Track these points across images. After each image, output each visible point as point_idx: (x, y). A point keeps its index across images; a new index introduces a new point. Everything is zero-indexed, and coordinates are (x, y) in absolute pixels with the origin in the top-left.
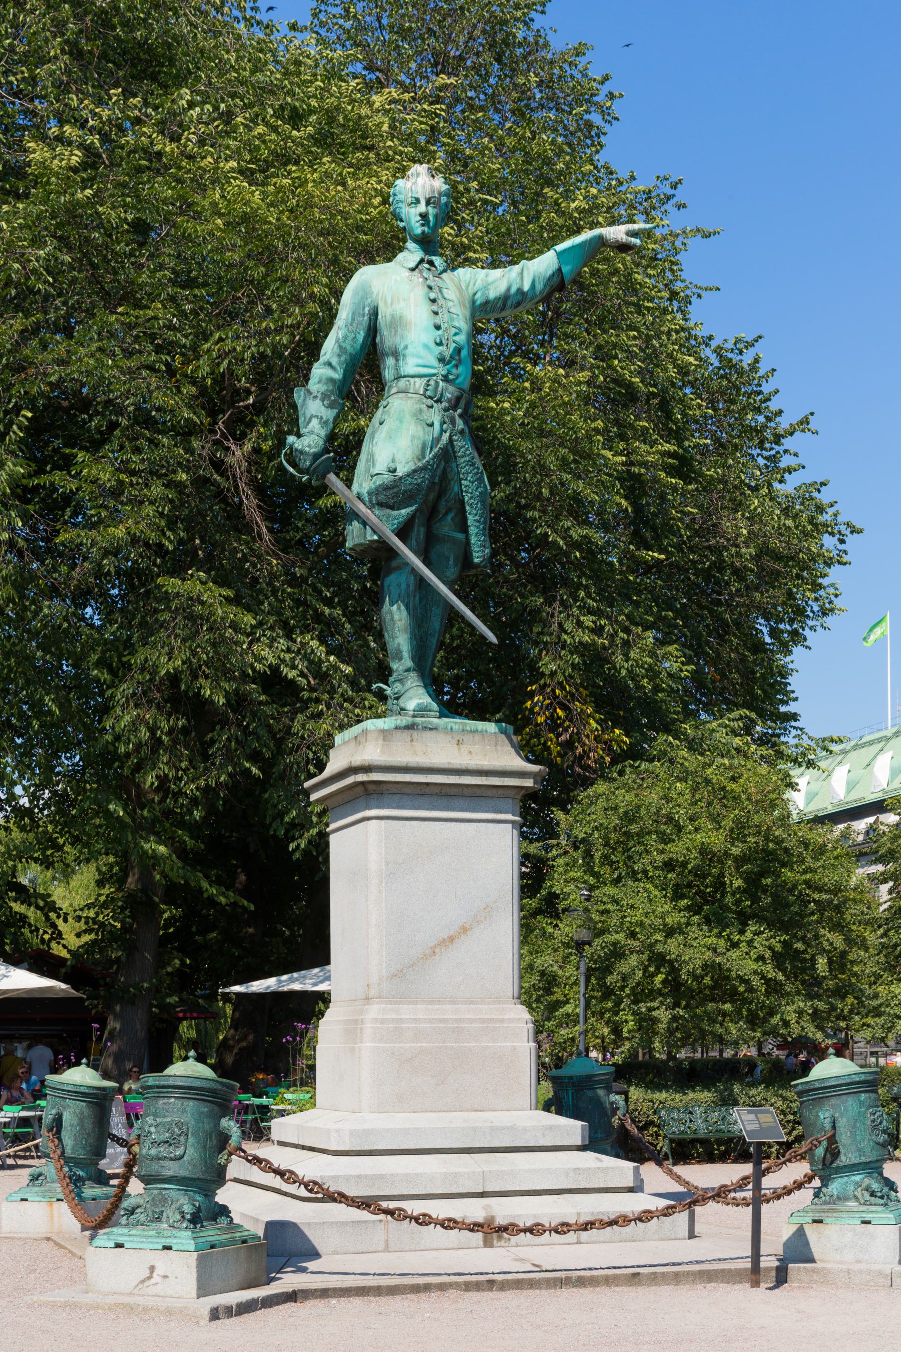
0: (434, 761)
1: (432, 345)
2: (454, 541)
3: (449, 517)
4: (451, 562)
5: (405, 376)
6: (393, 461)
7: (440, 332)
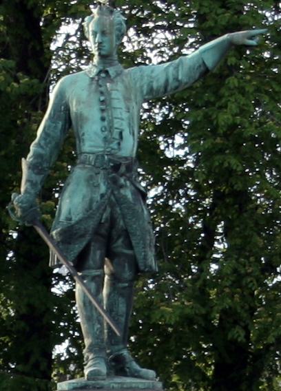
1: (99, 131)
2: (126, 255)
5: (84, 153)
6: (70, 213)
7: (106, 123)
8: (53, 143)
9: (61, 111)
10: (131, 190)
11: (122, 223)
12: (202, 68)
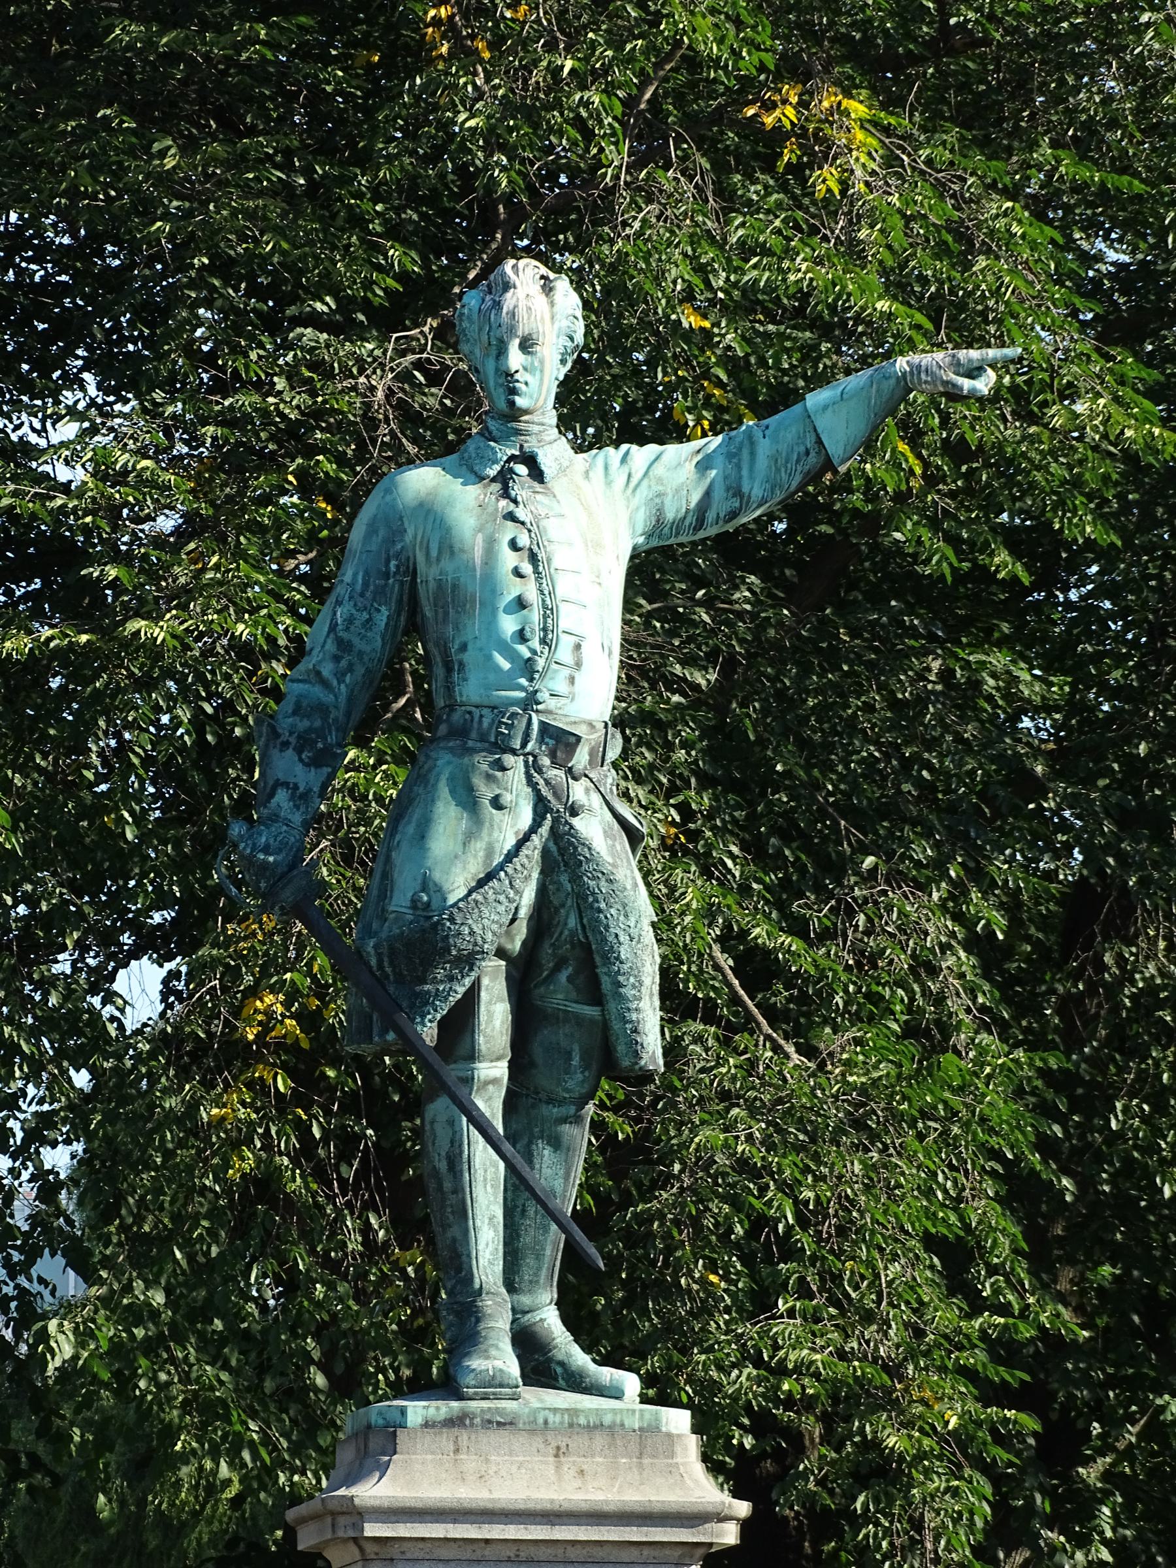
0: (496, 1495)
2: (579, 1020)
3: (563, 976)
4: (576, 1061)
8: (360, 670)
9: (387, 575)
10: (602, 821)
11: (572, 922)
12: (813, 459)
